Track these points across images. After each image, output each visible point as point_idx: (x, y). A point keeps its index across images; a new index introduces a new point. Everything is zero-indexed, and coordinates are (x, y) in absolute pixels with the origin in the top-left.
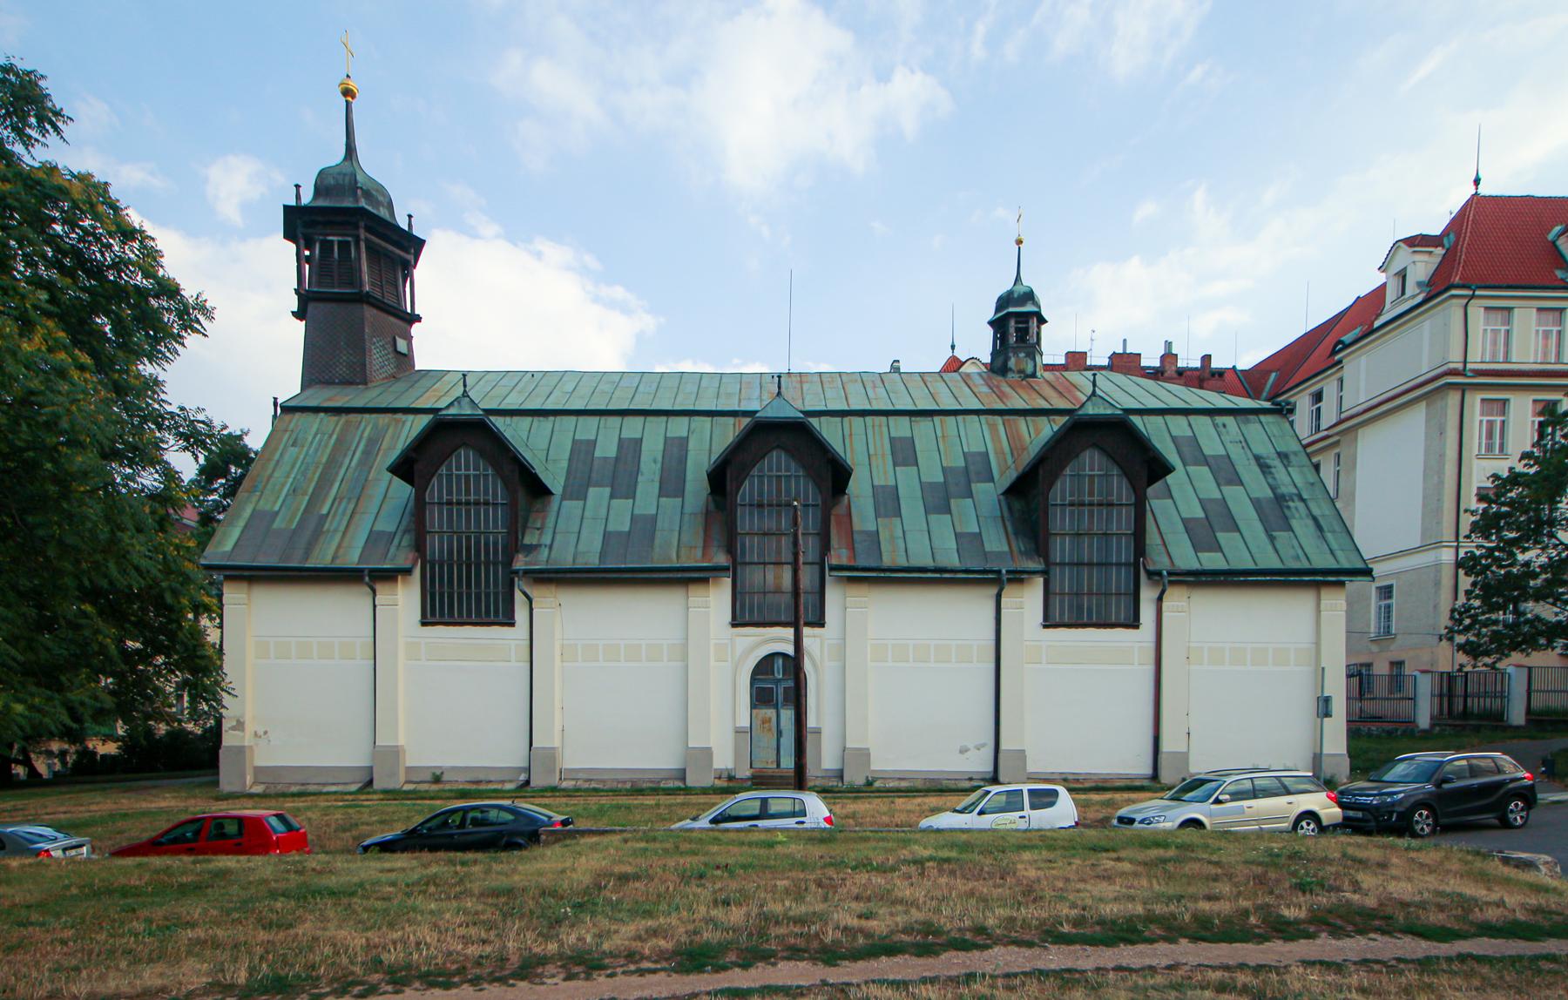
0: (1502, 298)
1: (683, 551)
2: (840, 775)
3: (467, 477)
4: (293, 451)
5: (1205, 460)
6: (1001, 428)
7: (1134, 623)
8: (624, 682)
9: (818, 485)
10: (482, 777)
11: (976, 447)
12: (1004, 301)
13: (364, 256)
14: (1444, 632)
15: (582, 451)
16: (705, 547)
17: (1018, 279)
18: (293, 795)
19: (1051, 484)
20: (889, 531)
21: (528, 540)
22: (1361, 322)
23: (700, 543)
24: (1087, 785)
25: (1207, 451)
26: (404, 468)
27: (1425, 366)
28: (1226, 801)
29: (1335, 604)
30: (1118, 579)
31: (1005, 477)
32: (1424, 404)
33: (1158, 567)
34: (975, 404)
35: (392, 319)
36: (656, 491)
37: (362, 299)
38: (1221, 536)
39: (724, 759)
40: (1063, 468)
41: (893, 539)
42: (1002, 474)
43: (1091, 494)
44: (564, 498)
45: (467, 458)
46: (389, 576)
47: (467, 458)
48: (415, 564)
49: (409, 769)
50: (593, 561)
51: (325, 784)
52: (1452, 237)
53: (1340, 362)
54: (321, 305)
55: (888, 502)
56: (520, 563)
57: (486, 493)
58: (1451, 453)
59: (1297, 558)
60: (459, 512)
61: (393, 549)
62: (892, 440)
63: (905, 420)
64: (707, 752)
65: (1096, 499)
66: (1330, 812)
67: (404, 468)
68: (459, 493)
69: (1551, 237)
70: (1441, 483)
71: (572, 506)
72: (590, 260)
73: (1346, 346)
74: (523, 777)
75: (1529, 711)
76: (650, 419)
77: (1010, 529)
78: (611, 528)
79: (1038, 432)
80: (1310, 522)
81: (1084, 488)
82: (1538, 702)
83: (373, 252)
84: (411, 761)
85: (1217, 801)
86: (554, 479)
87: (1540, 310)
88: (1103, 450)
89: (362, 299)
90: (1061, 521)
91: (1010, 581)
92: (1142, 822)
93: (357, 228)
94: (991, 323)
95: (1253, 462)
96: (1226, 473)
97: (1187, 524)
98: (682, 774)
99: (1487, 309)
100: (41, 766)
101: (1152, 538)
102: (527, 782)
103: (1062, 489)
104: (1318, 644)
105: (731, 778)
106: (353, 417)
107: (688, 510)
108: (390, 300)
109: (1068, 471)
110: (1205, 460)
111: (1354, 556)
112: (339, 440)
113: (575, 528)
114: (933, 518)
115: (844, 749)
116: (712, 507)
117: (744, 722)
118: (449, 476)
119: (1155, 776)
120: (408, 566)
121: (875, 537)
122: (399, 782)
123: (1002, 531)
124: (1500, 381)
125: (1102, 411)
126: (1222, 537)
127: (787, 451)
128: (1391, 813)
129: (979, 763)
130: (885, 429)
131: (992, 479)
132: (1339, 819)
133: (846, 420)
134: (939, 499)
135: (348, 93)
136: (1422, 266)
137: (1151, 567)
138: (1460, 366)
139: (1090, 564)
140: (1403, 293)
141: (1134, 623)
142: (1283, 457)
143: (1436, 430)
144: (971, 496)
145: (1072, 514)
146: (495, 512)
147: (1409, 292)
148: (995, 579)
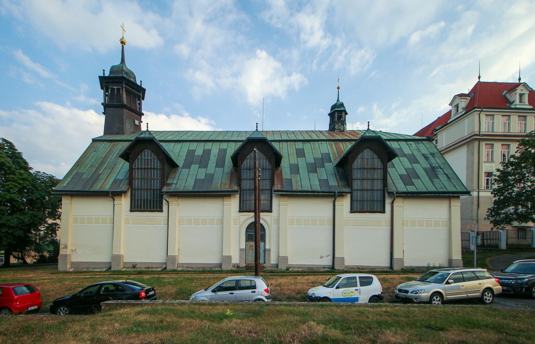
0: (490, 112)
1: (222, 186)
2: (277, 266)
3: (148, 159)
4: (94, 153)
5: (405, 156)
6: (334, 145)
7: (383, 211)
8: (200, 232)
9: (270, 162)
10: (150, 266)
12: (333, 107)
13: (124, 92)
14: (486, 217)
15: (191, 153)
16: (230, 184)
18: (84, 272)
19: (353, 161)
20: (295, 179)
21: (168, 182)
22: (444, 121)
23: (229, 183)
24: (367, 270)
25: (406, 153)
26: (126, 156)
27: (466, 133)
28: (452, 283)
29: (456, 205)
30: (377, 195)
31: (335, 160)
32: (466, 146)
33: (392, 191)
34: (325, 138)
35: (134, 114)
37: (124, 106)
38: (414, 180)
39: (236, 260)
40: (358, 156)
41: (297, 181)
42: (335, 160)
43: (367, 165)
44: (183, 168)
45: (148, 153)
47: (148, 153)
48: (128, 190)
49: (125, 263)
50: (191, 189)
51: (95, 268)
52: (472, 94)
53: (436, 134)
54: (110, 109)
55: (295, 169)
56: (165, 189)
57: (154, 165)
58: (476, 161)
59: (442, 188)
61: (121, 185)
62: (296, 149)
64: (230, 258)
65: (369, 167)
67: (126, 156)
69: (504, 94)
70: (473, 170)
71: (185, 171)
72: (213, 122)
73: (437, 130)
74: (164, 266)
75: (507, 245)
78: (197, 178)
79: (346, 147)
81: (364, 168)
82: (510, 241)
83: (128, 92)
84: (126, 260)
85: (448, 283)
86: (180, 162)
87: (519, 116)
88: (371, 149)
89: (124, 106)
90: (356, 174)
91: (339, 196)
92: (412, 293)
93: (122, 83)
95: (422, 156)
96: (413, 159)
97: (401, 176)
98: (220, 265)
99: (486, 115)
100: (29, 260)
101: (389, 181)
102: (166, 268)
103: (357, 163)
104: (450, 219)
105: (238, 267)
107: (225, 172)
109: (359, 157)
110: (405, 156)
111: (462, 187)
112: (110, 150)
113: (185, 179)
114: (310, 174)
115: (279, 256)
116: (233, 171)
117: (243, 246)
118: (141, 159)
119: (391, 267)
120: (125, 190)
121: (290, 181)
122: (121, 267)
124: (491, 138)
125: (371, 135)
126: (414, 181)
128: (522, 288)
129: (327, 262)
130: (294, 146)
131: (331, 162)
133: (281, 143)
134: (313, 168)
135: (123, 43)
136: (463, 104)
137: (389, 191)
138: (478, 133)
140: (457, 111)
141: (383, 211)
142: (432, 154)
143: (470, 154)
144: (324, 167)
147: (459, 111)
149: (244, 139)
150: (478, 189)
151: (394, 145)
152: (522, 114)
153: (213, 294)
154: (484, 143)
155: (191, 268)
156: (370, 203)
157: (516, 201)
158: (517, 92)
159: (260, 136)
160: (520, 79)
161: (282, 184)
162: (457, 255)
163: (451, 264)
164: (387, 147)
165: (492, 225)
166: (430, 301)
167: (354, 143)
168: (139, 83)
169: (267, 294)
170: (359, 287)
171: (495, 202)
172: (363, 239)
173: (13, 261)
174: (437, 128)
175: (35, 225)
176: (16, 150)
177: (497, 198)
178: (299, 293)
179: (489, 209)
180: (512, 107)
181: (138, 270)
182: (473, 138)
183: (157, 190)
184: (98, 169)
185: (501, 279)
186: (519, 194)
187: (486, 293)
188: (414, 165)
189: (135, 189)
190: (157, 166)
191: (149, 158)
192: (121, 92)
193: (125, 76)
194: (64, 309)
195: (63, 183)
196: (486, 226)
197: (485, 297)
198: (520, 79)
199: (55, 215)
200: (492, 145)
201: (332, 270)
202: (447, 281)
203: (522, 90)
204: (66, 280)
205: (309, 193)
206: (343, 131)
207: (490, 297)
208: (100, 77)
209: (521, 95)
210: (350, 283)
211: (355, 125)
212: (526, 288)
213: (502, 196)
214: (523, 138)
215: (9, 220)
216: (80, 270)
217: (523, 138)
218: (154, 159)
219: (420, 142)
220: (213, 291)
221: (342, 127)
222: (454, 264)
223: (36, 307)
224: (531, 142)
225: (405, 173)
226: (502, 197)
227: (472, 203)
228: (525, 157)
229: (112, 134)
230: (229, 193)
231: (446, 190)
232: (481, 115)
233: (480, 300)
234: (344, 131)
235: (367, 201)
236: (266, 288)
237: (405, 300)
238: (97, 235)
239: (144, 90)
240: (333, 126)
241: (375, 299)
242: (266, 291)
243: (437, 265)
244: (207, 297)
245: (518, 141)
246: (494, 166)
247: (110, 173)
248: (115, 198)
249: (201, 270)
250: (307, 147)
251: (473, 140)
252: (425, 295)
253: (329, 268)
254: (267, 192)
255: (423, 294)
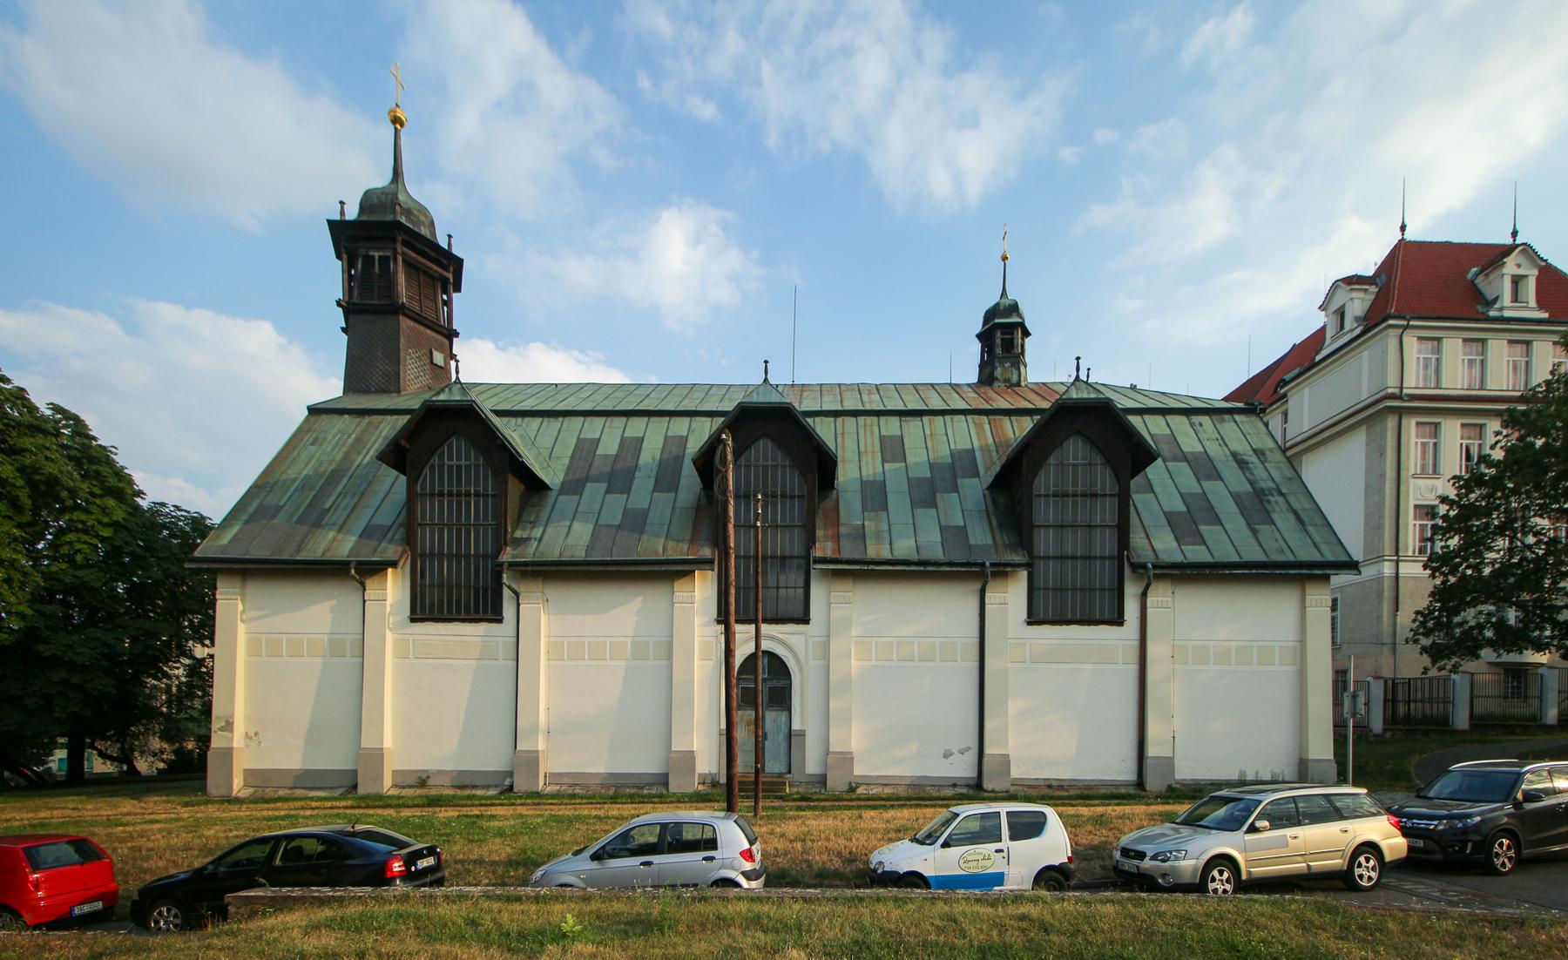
2: (822, 780)
3: (459, 467)
4: (313, 448)
5: (1185, 457)
7: (1118, 620)
8: (601, 680)
10: (467, 782)
11: (963, 444)
12: (990, 315)
13: (400, 268)
15: (586, 448)
17: (1004, 294)
19: (1035, 474)
21: (518, 534)
22: (1304, 359)
24: (1072, 793)
25: (1186, 449)
26: (397, 455)
27: (1364, 394)
29: (1319, 600)
30: (1102, 573)
32: (1364, 428)
33: (1142, 560)
34: (963, 406)
35: (429, 332)
36: (651, 486)
40: (1046, 456)
42: (987, 469)
46: (375, 569)
50: (580, 555)
52: (1384, 277)
53: (1285, 396)
56: (508, 555)
59: (1282, 551)
60: (459, 504)
62: (881, 438)
63: (895, 420)
65: (1080, 489)
66: (1394, 843)
68: (451, 484)
69: (1470, 276)
71: (568, 502)
73: (1286, 383)
74: (507, 782)
76: (653, 419)
77: (994, 522)
80: (1291, 516)
81: (1066, 493)
82: (1480, 708)
83: (408, 264)
85: (1253, 829)
86: (552, 474)
87: (1465, 340)
90: (1044, 512)
92: (1154, 858)
93: (395, 241)
94: (978, 336)
98: (663, 780)
99: (1420, 339)
100: (143, 765)
102: (511, 788)
103: (1045, 481)
104: (1302, 641)
106: (376, 418)
107: (680, 504)
108: (429, 314)
109: (1052, 460)
112: (357, 440)
114: (918, 511)
116: (703, 502)
118: (441, 467)
119: (1140, 783)
121: (861, 535)
123: (986, 525)
124: (1434, 406)
127: (773, 439)
128: (1464, 844)
129: (961, 768)
130: (876, 428)
131: (977, 475)
132: (1403, 853)
133: (839, 420)
134: (926, 493)
135: (396, 121)
136: (1358, 304)
137: (1135, 560)
138: (1397, 391)
139: (1074, 558)
140: (1342, 327)
141: (1118, 620)
144: (957, 491)
145: (1056, 504)
146: (486, 503)
147: (1347, 327)
148: (975, 572)
149: (729, 406)
150: (1397, 554)
151: (1150, 428)
152: (1520, 332)
153: (595, 865)
154: (1413, 422)
155: (582, 786)
156: (1081, 595)
157: (1495, 589)
158: (1505, 270)
159: (774, 398)
160: (1514, 234)
161: (837, 538)
162: (1321, 748)
163: (1304, 772)
164: (1130, 434)
165: (1426, 660)
166: (1199, 886)
167: (721, 420)
168: (444, 244)
169: (748, 866)
170: (1006, 843)
171: (1436, 594)
172: (1059, 703)
173: (98, 765)
174: (1287, 377)
175: (153, 662)
176: (95, 439)
177: (1438, 581)
178: (851, 859)
179: (1417, 613)
180: (1492, 313)
181: (433, 792)
182: (1381, 406)
183: (485, 556)
184: (321, 494)
185: (1410, 816)
186: (1503, 571)
187: (1362, 859)
188: (1207, 484)
189: (423, 556)
190: (486, 488)
191: (455, 462)
192: (392, 267)
193: (403, 220)
194: (169, 911)
195: (218, 537)
196: (1412, 664)
197: (1357, 871)
198: (1514, 234)
199: (206, 631)
200: (1437, 425)
201: (976, 789)
202: (1253, 824)
203: (1519, 266)
204: (211, 822)
205: (913, 568)
206: (1014, 385)
207: (1373, 869)
208: (331, 223)
209: (1517, 281)
210: (986, 832)
211: (1047, 365)
212: (1475, 844)
213: (1452, 573)
214: (1512, 406)
215: (70, 647)
216: (270, 793)
217: (1512, 406)
218: (477, 466)
219: (1227, 417)
220: (596, 857)
221: (1015, 373)
222: (1312, 771)
223: (99, 905)
224: (1533, 416)
225: (1181, 507)
226: (1452, 580)
227: (1380, 596)
228: (1518, 459)
229: (366, 391)
230: (686, 568)
231: (1291, 558)
232: (1405, 338)
233: (1342, 881)
234: (1018, 384)
235: (1074, 589)
236: (746, 845)
237: (1129, 877)
238: (314, 689)
239: (459, 263)
240: (988, 370)
241: (1052, 878)
242: (747, 855)
243: (1268, 777)
244: (577, 874)
245: (1497, 413)
246: (1429, 488)
247: (355, 506)
248: (368, 583)
249: (611, 792)
250: (913, 427)
251: (1385, 410)
252: (1189, 863)
253: (968, 786)
254: (795, 562)
255: (1183, 863)
